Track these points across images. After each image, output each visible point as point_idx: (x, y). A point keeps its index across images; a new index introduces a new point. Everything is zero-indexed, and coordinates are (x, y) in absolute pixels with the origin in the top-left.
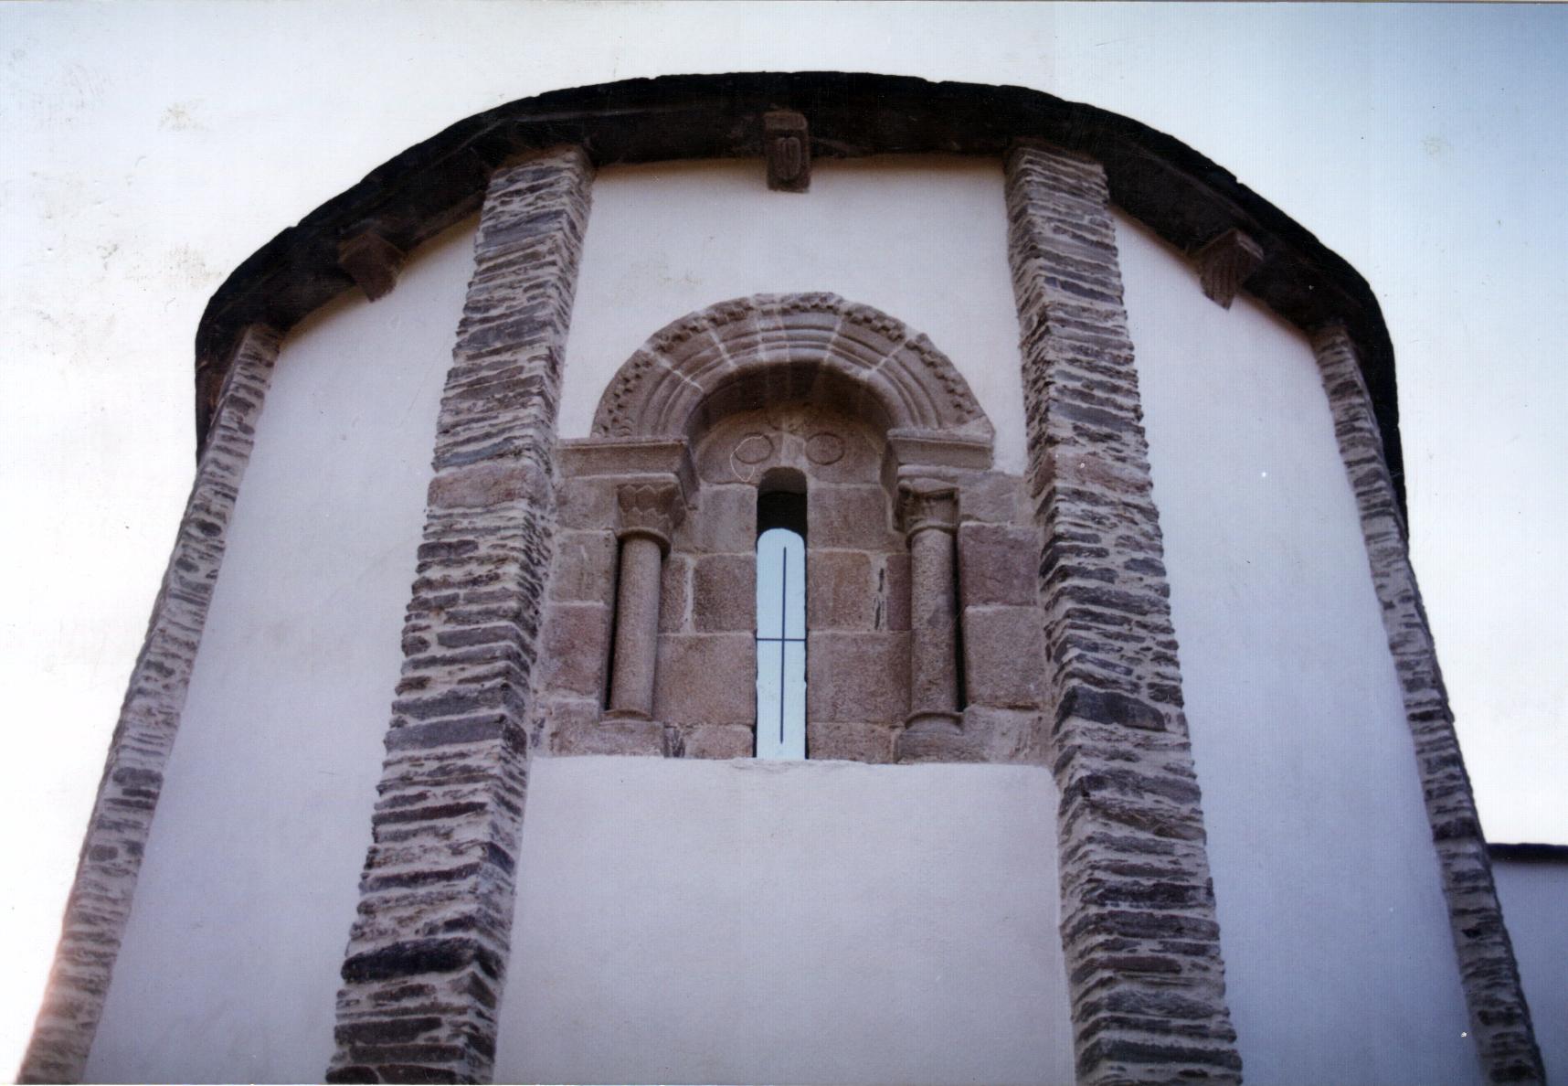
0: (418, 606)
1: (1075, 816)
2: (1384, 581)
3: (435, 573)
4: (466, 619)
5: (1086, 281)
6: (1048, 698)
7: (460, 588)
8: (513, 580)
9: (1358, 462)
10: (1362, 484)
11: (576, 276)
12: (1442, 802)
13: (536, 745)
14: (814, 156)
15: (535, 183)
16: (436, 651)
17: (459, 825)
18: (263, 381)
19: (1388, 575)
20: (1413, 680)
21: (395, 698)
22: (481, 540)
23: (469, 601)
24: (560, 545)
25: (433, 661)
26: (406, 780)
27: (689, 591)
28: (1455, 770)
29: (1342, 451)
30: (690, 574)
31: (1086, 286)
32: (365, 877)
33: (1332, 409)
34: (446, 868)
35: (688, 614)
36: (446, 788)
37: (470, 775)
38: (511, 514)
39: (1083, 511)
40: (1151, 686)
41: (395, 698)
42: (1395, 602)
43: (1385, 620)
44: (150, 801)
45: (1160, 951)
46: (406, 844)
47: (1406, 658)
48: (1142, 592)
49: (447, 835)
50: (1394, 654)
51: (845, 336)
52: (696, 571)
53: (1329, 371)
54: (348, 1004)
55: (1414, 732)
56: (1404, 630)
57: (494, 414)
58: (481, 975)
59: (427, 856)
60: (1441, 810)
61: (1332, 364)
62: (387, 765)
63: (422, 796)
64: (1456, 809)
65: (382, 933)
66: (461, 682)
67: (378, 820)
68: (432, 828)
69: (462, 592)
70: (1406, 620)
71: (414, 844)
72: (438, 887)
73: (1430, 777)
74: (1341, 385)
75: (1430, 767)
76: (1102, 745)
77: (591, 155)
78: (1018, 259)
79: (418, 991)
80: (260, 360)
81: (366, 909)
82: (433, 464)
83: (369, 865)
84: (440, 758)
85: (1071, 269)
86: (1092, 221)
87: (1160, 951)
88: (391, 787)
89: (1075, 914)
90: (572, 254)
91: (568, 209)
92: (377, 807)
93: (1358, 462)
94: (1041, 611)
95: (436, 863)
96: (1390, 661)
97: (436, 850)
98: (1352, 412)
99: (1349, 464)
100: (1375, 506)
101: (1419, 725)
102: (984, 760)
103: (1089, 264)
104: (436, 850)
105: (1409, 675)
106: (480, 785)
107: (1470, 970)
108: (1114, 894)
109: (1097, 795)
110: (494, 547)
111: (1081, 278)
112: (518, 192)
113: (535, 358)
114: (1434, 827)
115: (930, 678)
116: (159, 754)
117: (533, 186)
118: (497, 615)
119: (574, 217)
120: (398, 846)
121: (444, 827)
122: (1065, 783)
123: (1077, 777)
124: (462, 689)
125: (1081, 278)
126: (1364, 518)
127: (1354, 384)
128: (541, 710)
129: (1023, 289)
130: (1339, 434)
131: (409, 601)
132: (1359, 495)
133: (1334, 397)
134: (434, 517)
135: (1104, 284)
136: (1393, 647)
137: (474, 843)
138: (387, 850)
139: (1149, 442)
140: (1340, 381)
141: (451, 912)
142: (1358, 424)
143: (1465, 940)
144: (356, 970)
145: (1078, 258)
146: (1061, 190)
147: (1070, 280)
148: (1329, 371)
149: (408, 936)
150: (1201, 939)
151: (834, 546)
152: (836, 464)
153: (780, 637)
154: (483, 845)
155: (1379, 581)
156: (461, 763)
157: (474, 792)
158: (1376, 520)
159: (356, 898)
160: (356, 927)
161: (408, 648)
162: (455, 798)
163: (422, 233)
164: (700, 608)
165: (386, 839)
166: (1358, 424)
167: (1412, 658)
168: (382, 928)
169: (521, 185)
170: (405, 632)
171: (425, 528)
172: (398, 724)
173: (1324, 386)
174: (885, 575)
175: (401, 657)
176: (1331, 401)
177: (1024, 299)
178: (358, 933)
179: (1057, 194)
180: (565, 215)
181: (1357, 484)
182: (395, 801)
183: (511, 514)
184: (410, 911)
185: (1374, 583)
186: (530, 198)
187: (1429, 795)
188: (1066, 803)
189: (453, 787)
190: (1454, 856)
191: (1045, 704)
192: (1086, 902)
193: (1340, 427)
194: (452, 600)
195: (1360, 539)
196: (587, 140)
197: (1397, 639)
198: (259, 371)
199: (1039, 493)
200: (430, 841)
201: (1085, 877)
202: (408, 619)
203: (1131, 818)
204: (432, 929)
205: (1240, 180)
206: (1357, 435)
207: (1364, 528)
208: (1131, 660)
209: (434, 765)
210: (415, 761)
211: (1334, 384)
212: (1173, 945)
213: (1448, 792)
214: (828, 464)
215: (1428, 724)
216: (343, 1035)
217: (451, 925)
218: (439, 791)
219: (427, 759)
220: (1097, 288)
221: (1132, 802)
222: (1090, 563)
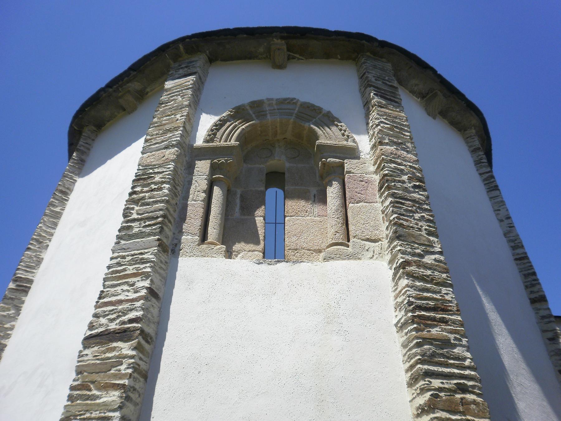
0: (131, 201)
1: (400, 278)
2: (498, 212)
3: (138, 189)
4: (148, 204)
5: (388, 95)
6: (384, 236)
7: (147, 193)
8: (167, 189)
9: (483, 174)
10: (486, 180)
11: (200, 94)
12: (532, 289)
13: (173, 253)
14: (288, 59)
15: (188, 65)
16: (135, 216)
17: (138, 281)
18: (90, 145)
19: (499, 210)
20: (515, 246)
21: (118, 233)
22: (156, 176)
23: (150, 198)
24: (187, 182)
25: (134, 220)
26: (119, 264)
27: (238, 201)
28: (534, 277)
29: (477, 170)
30: (238, 196)
31: (388, 97)
32: (97, 302)
33: (472, 157)
34: (131, 298)
35: (237, 209)
36: (134, 266)
37: (143, 261)
38: (168, 166)
39: (394, 166)
40: (426, 229)
41: (118, 233)
42: (504, 219)
43: (501, 226)
44: (27, 289)
45: (440, 331)
46: (116, 289)
47: (511, 238)
48: (419, 196)
49: (133, 285)
50: (506, 237)
51: (300, 112)
52: (241, 195)
53: (470, 144)
54: (82, 356)
55: (517, 264)
56: (508, 229)
57: (165, 135)
58: (143, 342)
59: (124, 293)
60: (532, 292)
61: (471, 142)
62: (112, 259)
63: (124, 270)
64: (538, 292)
65: (101, 325)
66: (144, 227)
67: (105, 280)
68: (126, 282)
69: (147, 194)
70: (508, 225)
71: (119, 289)
72: (126, 306)
73: (527, 280)
74: (475, 149)
75: (526, 276)
76: (409, 250)
77: (209, 58)
78: (363, 89)
79: (113, 349)
80: (90, 138)
81: (96, 316)
82: (141, 152)
83: (100, 298)
84: (132, 255)
85: (382, 91)
86: (388, 79)
87: (440, 331)
88: (112, 267)
89: (402, 318)
90: (199, 86)
91: (199, 72)
92: (106, 274)
93: (483, 174)
94: (380, 205)
95: (127, 296)
96: (505, 239)
97: (128, 291)
98: (480, 157)
99: (480, 174)
100: (492, 187)
101: (519, 262)
102: (359, 259)
103: (389, 91)
104: (128, 291)
105: (513, 244)
106: (148, 265)
107: (552, 353)
108: (420, 308)
109: (409, 269)
110: (161, 178)
111: (386, 95)
112: (182, 68)
113: (183, 116)
114: (530, 299)
115: (336, 230)
116: (34, 273)
117: (187, 66)
118: (160, 202)
119: (202, 76)
120: (113, 290)
121: (131, 281)
122: (394, 266)
123: (400, 262)
124: (144, 230)
125: (386, 95)
126: (488, 192)
127: (480, 149)
128: (176, 240)
129: (365, 98)
130: (476, 164)
131: (127, 199)
132: (485, 184)
133: (472, 153)
134: (140, 170)
135: (394, 97)
136: (505, 235)
137: (143, 287)
138: (108, 291)
139: (416, 147)
140: (474, 147)
141: (132, 315)
142: (482, 161)
143: (548, 341)
144: (88, 341)
145: (385, 89)
146: (377, 69)
147: (383, 95)
148: (470, 144)
149: (113, 326)
150: (457, 327)
151: (296, 186)
152: (297, 158)
153: (275, 222)
154: (147, 288)
155: (497, 212)
156: (141, 257)
157: (144, 268)
158: (493, 192)
159: (93, 311)
160: (91, 323)
161: (125, 216)
162: (137, 270)
163: (148, 90)
164: (242, 208)
165: (108, 287)
166: (482, 161)
167: (514, 238)
168: (101, 323)
169: (183, 66)
170: (124, 210)
171: (136, 174)
172: (117, 243)
173: (468, 150)
174: (316, 196)
175: (122, 219)
176: (471, 154)
177: (366, 101)
178: (91, 327)
179: (376, 70)
180: (197, 73)
181: (485, 180)
182: (113, 272)
183: (168, 166)
184: (114, 316)
185: (495, 213)
186: (186, 69)
187: (526, 287)
188: (395, 275)
189: (137, 266)
190: (540, 309)
191: (383, 238)
192: (407, 312)
193: (475, 162)
194: (143, 198)
195: (487, 199)
196: (208, 52)
197: (506, 232)
198: (89, 141)
199: (376, 164)
200: (126, 287)
201: (406, 302)
202: (126, 205)
203: (422, 278)
204: (124, 323)
205: (438, 73)
206: (482, 164)
207: (488, 195)
208: (418, 220)
209: (130, 258)
210: (123, 257)
211: (472, 148)
212: (445, 329)
213: (533, 286)
214: (294, 158)
215: (522, 261)
216: (79, 372)
217: (131, 321)
218: (131, 268)
219: (128, 256)
220: (392, 98)
221: (423, 272)
222: (399, 185)
